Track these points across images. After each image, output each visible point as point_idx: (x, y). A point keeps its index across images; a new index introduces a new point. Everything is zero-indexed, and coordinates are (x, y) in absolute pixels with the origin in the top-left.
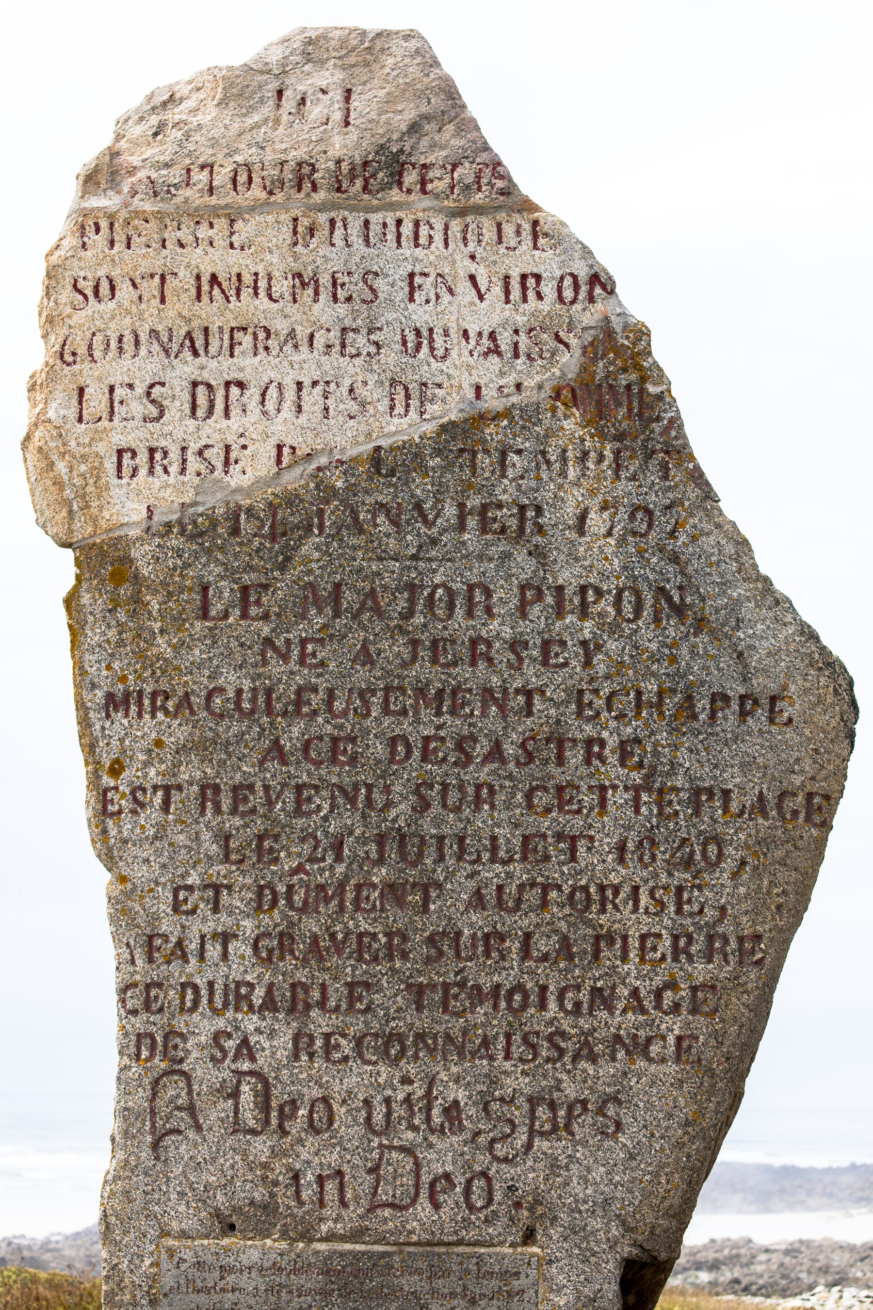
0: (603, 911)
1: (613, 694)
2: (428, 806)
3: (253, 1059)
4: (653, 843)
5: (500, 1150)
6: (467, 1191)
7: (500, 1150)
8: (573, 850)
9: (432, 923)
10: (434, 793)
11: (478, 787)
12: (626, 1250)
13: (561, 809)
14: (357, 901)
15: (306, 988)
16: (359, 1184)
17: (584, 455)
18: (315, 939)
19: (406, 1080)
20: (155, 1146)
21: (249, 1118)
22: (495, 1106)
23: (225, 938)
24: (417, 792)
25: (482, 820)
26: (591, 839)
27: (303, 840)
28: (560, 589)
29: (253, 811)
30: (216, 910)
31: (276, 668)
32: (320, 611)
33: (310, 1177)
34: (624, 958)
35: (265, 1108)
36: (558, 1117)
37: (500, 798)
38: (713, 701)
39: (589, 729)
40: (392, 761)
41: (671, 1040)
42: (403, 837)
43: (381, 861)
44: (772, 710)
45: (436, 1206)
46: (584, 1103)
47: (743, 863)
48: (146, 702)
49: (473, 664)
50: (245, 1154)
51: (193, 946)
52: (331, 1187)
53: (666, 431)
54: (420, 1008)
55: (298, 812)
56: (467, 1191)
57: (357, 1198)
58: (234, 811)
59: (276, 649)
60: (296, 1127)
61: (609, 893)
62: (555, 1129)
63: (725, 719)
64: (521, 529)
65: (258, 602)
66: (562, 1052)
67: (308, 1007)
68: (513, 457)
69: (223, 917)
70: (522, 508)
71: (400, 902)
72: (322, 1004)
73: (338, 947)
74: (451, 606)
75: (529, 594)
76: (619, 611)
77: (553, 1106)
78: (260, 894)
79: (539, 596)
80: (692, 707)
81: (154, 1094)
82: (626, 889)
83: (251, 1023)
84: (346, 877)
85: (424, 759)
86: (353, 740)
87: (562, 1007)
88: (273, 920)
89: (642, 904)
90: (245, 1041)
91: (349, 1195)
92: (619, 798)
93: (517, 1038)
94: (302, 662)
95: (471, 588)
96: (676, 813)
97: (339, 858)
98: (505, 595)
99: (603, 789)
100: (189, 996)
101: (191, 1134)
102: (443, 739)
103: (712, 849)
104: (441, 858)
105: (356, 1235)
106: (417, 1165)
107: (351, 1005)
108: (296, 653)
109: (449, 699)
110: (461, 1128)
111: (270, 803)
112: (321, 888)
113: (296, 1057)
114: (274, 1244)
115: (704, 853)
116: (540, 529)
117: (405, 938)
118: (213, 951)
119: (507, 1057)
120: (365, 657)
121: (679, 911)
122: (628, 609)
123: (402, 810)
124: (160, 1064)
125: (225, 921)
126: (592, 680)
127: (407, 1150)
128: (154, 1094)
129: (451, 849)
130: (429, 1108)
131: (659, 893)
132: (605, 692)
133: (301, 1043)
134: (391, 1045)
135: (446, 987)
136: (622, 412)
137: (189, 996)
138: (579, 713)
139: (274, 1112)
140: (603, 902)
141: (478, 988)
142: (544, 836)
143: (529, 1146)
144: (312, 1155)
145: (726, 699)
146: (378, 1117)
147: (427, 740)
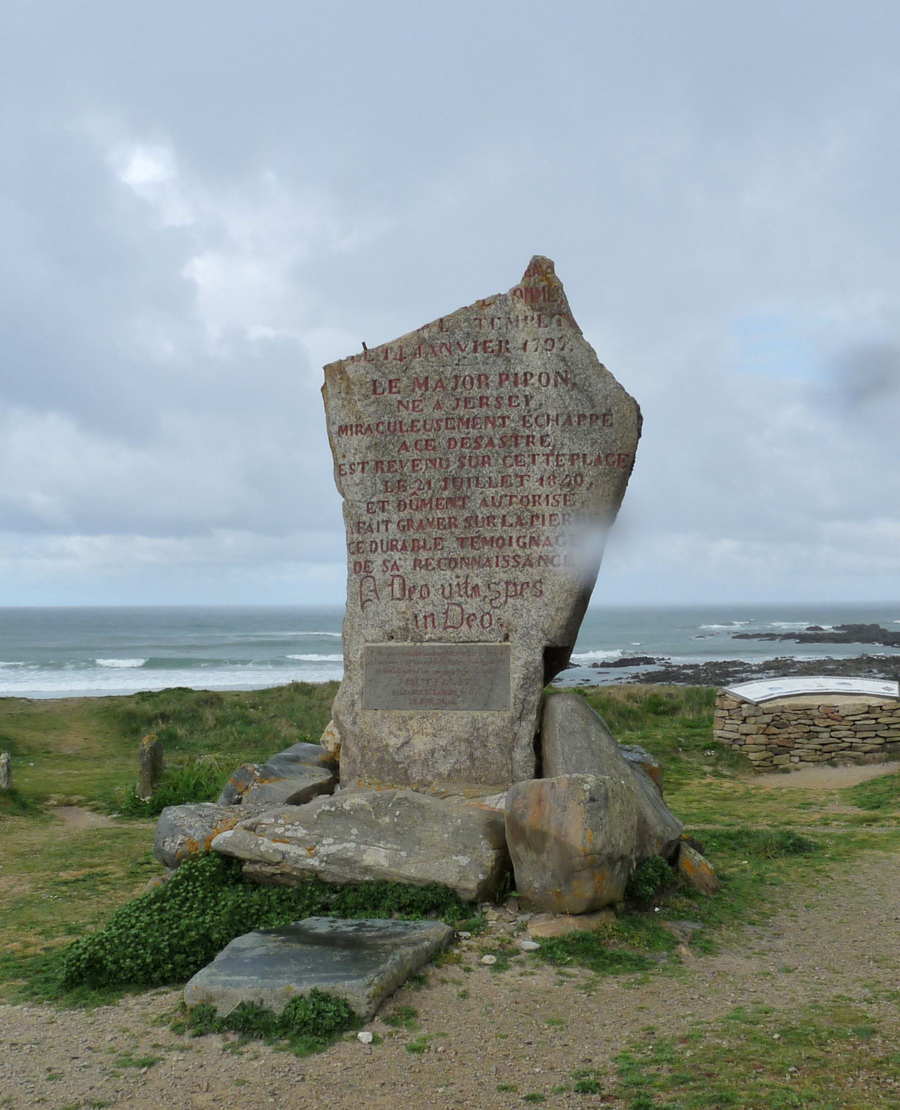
0: (534, 505)
1: (538, 416)
2: (464, 465)
3: (398, 570)
4: (555, 477)
5: (495, 604)
6: (482, 620)
7: (495, 604)
8: (522, 481)
9: (467, 514)
10: (466, 461)
11: (484, 457)
12: (544, 643)
13: (517, 465)
14: (437, 505)
15: (418, 541)
16: (440, 620)
17: (526, 318)
18: (421, 521)
19: (458, 577)
20: (362, 606)
21: (397, 593)
22: (492, 586)
23: (387, 522)
24: (459, 460)
25: (486, 470)
26: (529, 476)
27: (415, 482)
28: (516, 374)
29: (396, 471)
30: (383, 511)
31: (404, 413)
32: (420, 388)
33: (421, 617)
34: (543, 524)
35: (404, 589)
36: (516, 589)
37: (493, 461)
38: (579, 418)
39: (528, 432)
40: (449, 448)
41: (562, 557)
42: (454, 478)
43: (445, 488)
44: (604, 420)
45: (470, 627)
46: (528, 583)
47: (592, 484)
48: (354, 429)
49: (481, 407)
50: (396, 609)
51: (375, 526)
52: (429, 620)
53: (560, 306)
54: (462, 547)
55: (414, 471)
56: (482, 620)
57: (439, 625)
58: (389, 470)
59: (403, 405)
60: (416, 596)
61: (537, 498)
62: (516, 595)
63: (584, 424)
64: (500, 350)
65: (396, 386)
66: (518, 563)
67: (419, 548)
68: (496, 320)
69: (386, 514)
70: (500, 342)
71: (454, 505)
72: (424, 547)
73: (431, 524)
74: (472, 384)
75: (504, 377)
76: (540, 382)
77: (515, 584)
78: (399, 505)
79: (507, 378)
80: (570, 421)
81: (361, 585)
82: (544, 496)
83: (396, 555)
84: (432, 496)
85: (462, 446)
86: (434, 440)
87: (518, 545)
88: (405, 514)
89: (550, 502)
90: (395, 563)
91: (436, 624)
92: (540, 459)
93: (501, 559)
94: (413, 410)
95: (480, 376)
96: (564, 465)
97: (429, 488)
98: (494, 379)
99: (534, 456)
100: (374, 546)
101: (376, 601)
102: (469, 438)
103: (579, 479)
104: (469, 486)
105: (440, 639)
106: (462, 610)
107: (436, 547)
108: (411, 406)
109: (468, 423)
110: (479, 595)
111: (402, 467)
112: (423, 500)
113: (415, 568)
114: (408, 644)
115: (575, 480)
116: (508, 350)
117: (456, 519)
118: (382, 527)
119: (497, 566)
120: (438, 406)
121: (565, 504)
122: (544, 381)
123: (453, 467)
124: (363, 574)
125: (383, 516)
126: (529, 411)
127: (459, 605)
128: (361, 585)
129: (473, 483)
130: (466, 588)
131: (557, 498)
132: (534, 416)
133: (417, 563)
134: (452, 563)
135: (472, 538)
136: (542, 298)
137: (374, 546)
138: (524, 425)
139: (408, 591)
140: (534, 502)
141: (485, 538)
142: (510, 476)
143: (506, 601)
144: (423, 608)
145: (584, 416)
146: (447, 592)
147: (463, 438)
